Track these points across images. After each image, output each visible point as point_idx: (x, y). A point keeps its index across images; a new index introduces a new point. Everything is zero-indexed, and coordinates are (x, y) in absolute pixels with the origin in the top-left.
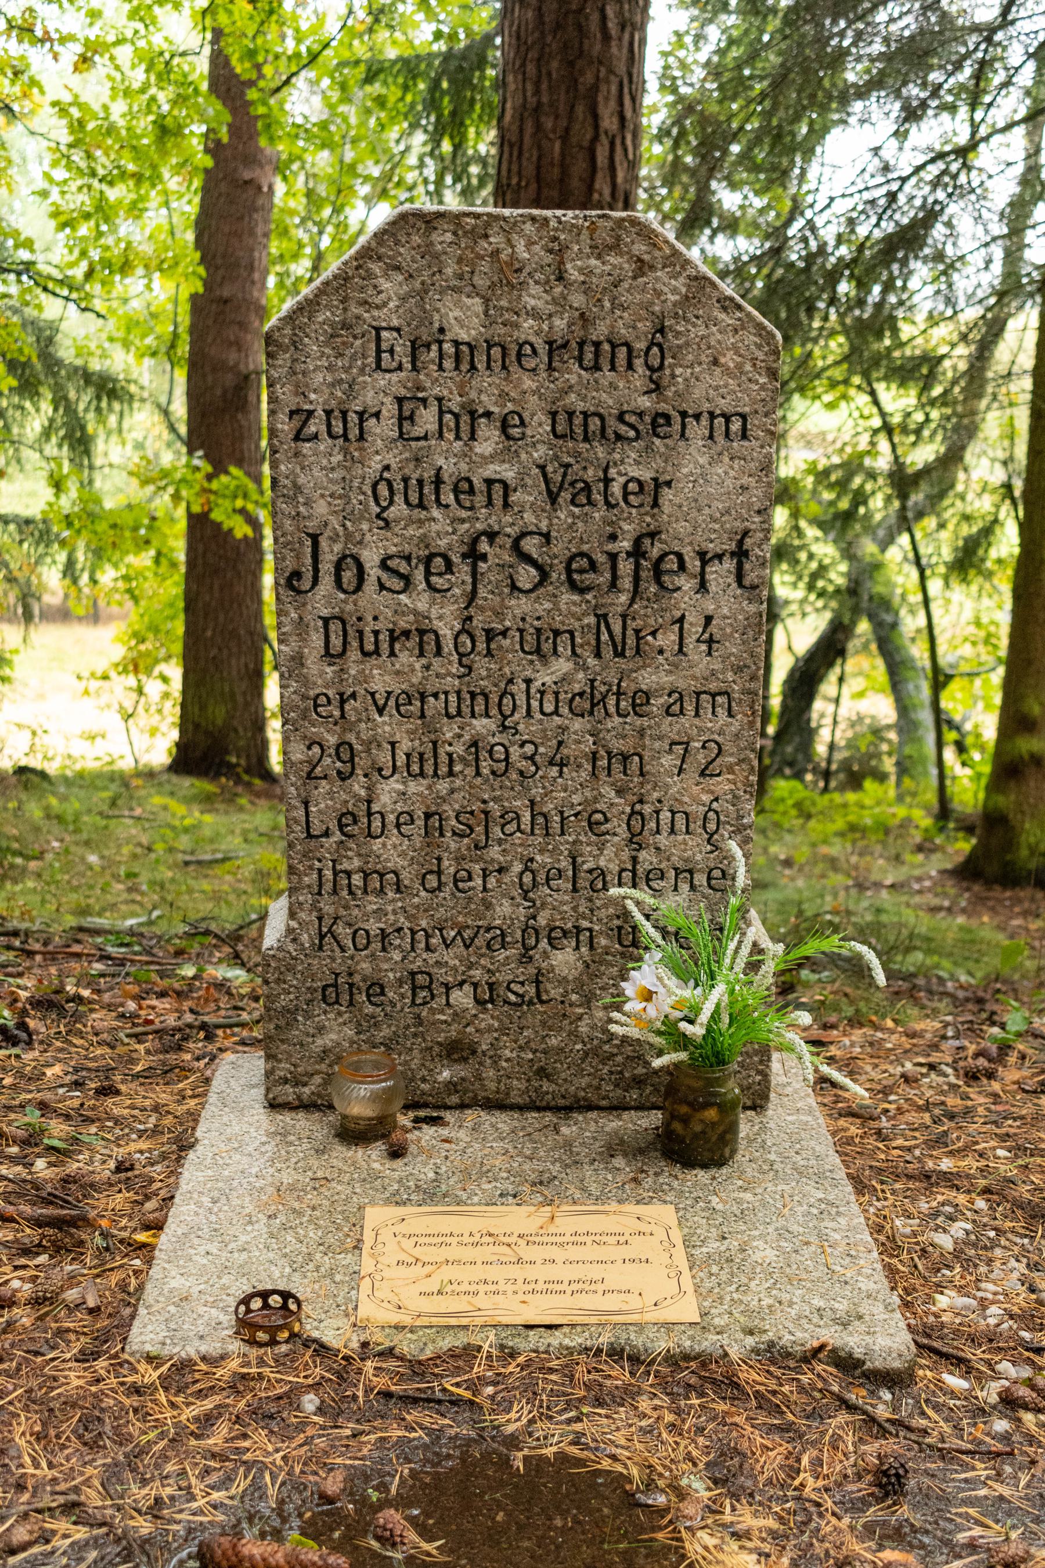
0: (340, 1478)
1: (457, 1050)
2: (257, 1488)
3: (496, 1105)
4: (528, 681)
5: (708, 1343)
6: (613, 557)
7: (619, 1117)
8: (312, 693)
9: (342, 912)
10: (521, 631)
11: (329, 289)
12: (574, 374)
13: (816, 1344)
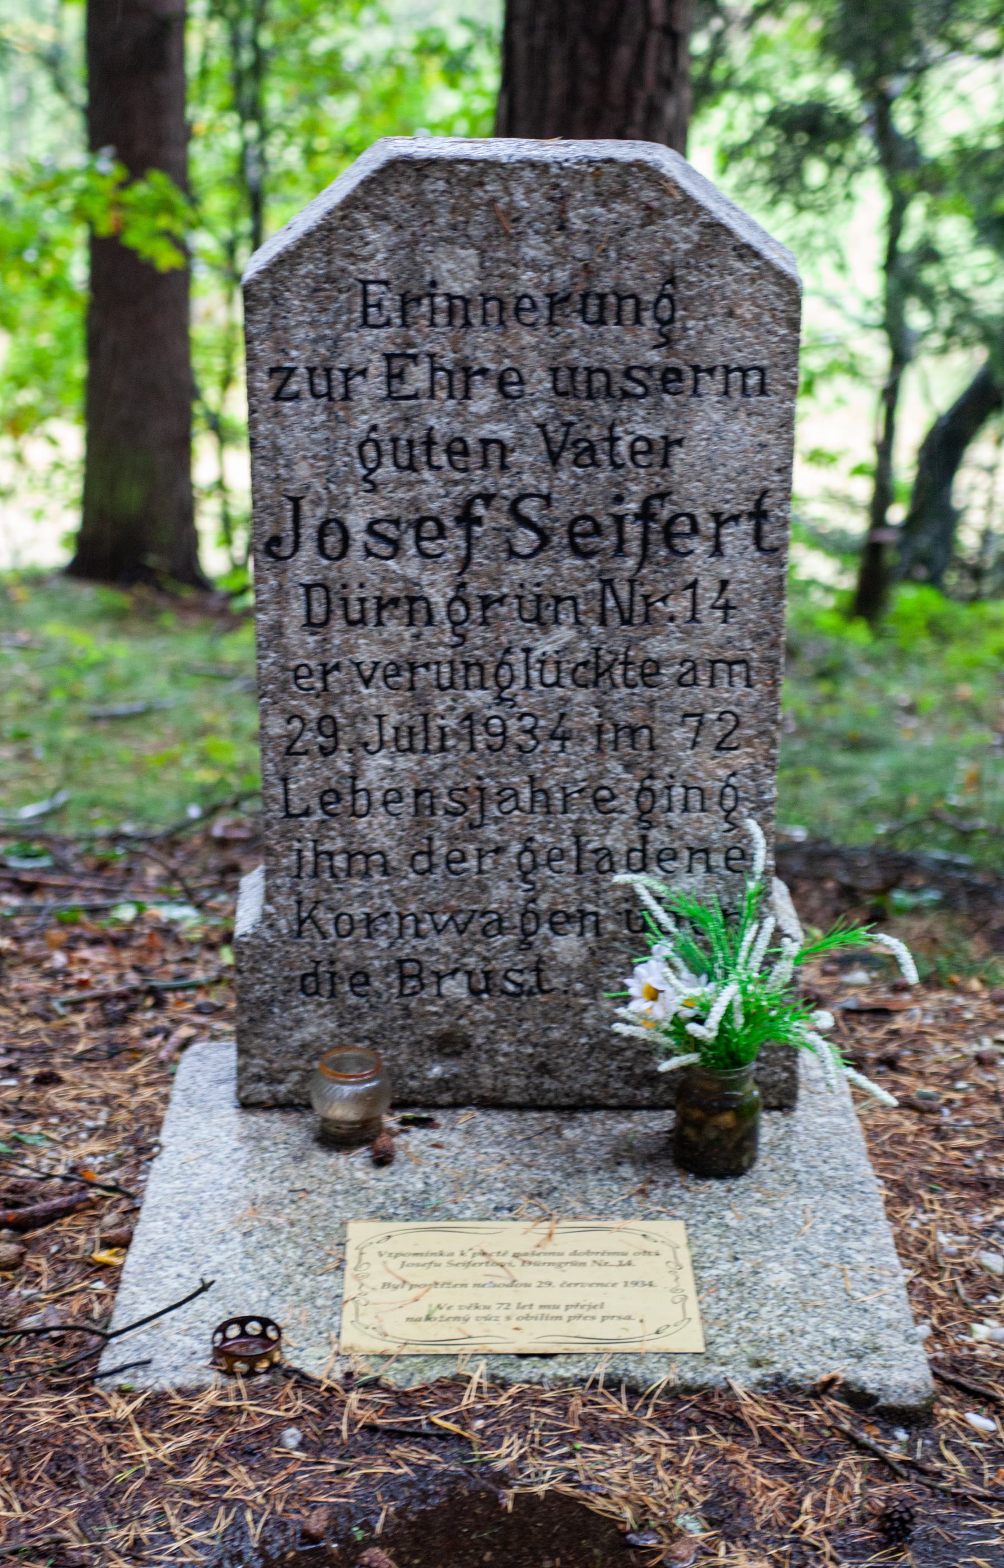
0: (324, 1516)
1: (450, 1044)
2: (238, 1527)
3: (492, 1103)
4: (527, 651)
5: (711, 1374)
6: (619, 520)
7: (628, 1118)
8: (293, 664)
9: (324, 896)
10: (519, 597)
11: (312, 241)
12: (576, 328)
13: (825, 1377)
